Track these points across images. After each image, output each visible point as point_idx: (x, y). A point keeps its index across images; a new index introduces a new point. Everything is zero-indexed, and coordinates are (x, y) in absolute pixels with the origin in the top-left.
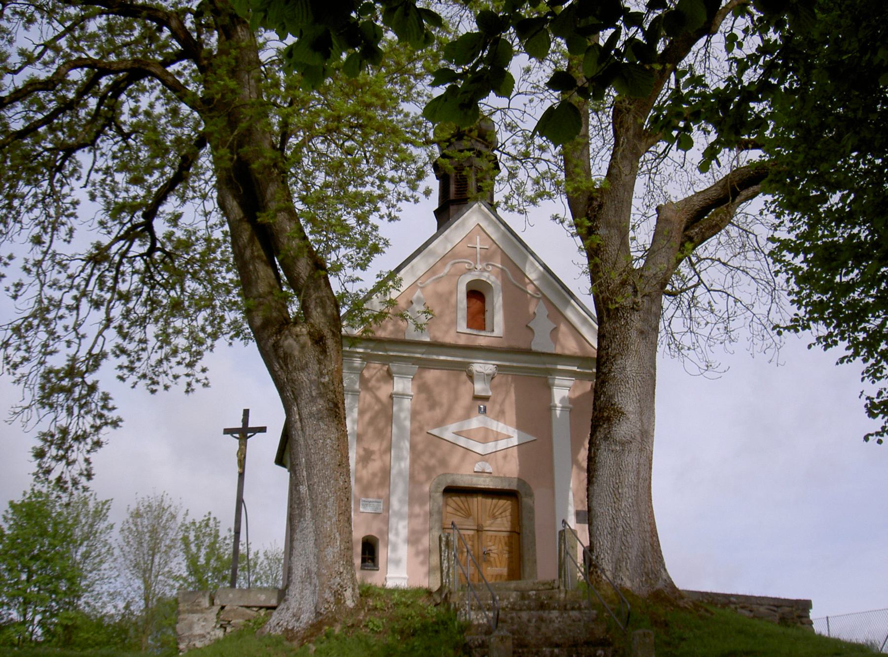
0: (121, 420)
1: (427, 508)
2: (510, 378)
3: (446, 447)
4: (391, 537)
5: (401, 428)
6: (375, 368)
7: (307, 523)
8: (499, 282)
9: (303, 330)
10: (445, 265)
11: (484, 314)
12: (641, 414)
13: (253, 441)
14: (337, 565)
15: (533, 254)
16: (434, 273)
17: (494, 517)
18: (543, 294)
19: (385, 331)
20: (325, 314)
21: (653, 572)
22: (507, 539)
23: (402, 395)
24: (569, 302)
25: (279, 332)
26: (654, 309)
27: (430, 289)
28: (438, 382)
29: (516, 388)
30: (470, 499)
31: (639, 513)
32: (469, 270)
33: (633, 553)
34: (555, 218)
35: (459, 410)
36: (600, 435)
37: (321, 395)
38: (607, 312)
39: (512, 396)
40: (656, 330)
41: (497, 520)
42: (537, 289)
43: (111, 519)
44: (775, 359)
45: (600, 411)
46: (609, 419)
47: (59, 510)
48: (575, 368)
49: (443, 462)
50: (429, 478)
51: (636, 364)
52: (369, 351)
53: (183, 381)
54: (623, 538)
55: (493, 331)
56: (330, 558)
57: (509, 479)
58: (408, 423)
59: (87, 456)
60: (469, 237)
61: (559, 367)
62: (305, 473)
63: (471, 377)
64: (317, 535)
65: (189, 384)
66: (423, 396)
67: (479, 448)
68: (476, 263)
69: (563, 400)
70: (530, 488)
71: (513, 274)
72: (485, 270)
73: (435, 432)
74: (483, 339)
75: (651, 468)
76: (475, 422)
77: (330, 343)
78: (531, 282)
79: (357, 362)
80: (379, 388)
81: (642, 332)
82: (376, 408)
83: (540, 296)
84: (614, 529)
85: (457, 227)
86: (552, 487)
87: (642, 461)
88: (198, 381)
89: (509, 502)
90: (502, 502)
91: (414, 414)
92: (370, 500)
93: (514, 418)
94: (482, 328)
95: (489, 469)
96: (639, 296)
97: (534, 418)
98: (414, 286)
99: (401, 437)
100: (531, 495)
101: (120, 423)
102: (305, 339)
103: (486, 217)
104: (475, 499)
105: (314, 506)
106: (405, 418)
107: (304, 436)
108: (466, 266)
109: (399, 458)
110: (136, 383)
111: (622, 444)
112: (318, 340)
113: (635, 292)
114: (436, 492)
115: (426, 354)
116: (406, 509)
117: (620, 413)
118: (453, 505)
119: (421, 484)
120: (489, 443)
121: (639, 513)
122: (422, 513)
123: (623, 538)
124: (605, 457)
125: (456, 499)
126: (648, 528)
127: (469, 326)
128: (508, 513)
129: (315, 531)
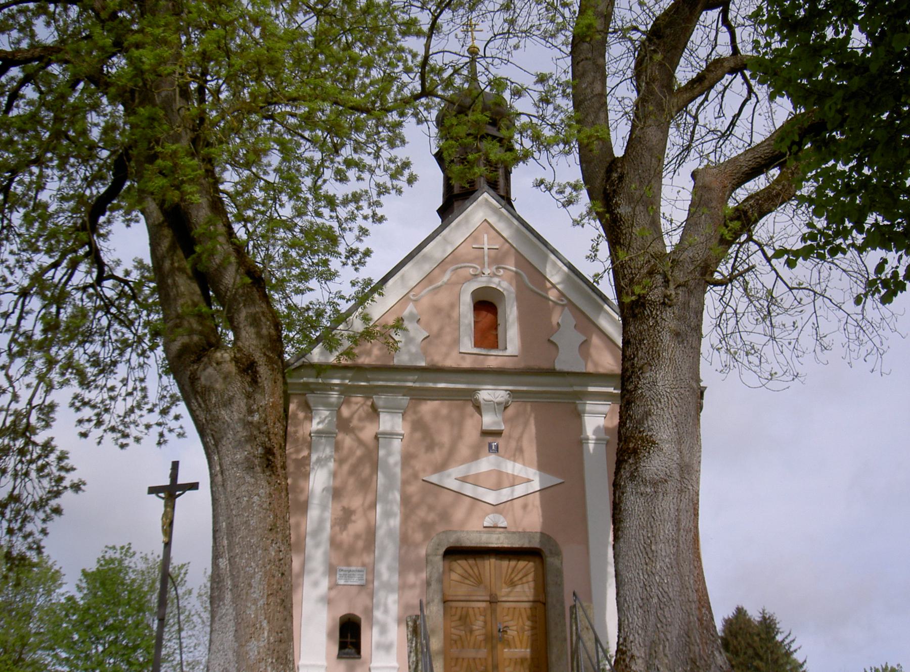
0: (84, 484)
1: (424, 575)
2: (529, 408)
3: (446, 498)
4: (378, 614)
5: (390, 476)
6: (357, 403)
7: (227, 609)
8: (513, 289)
9: (226, 355)
10: (444, 272)
11: (496, 329)
12: (680, 442)
13: (183, 501)
14: (263, 664)
15: (554, 252)
16: (431, 282)
17: (512, 584)
18: (569, 301)
19: (372, 354)
20: (259, 335)
21: (701, 657)
22: (529, 612)
23: (390, 435)
24: (602, 308)
25: (198, 360)
26: (693, 303)
27: (425, 302)
28: (436, 414)
29: (535, 418)
30: (480, 562)
31: (681, 576)
32: (475, 275)
33: (674, 633)
34: (540, 183)
35: (464, 450)
36: (625, 473)
37: (251, 439)
38: (632, 311)
39: (532, 428)
40: (698, 329)
41: (517, 589)
42: (562, 294)
43: (189, 585)
44: (878, 368)
45: (625, 441)
46: (635, 452)
47: (133, 577)
48: (611, 390)
49: (445, 516)
50: (427, 537)
51: (670, 377)
52: (347, 381)
53: (156, 430)
54: (660, 612)
55: (506, 348)
56: (253, 655)
57: (524, 533)
58: (398, 470)
59: (44, 526)
60: (474, 237)
61: (591, 389)
62: (225, 542)
63: (478, 408)
64: (237, 624)
65: (161, 435)
66: (418, 435)
67: (490, 497)
68: (483, 267)
69: (597, 431)
70: (557, 545)
71: (531, 277)
72: (495, 275)
73: (434, 478)
74: (493, 360)
75: (696, 515)
76: (486, 464)
77: (263, 370)
78: (554, 286)
79: (334, 396)
80: (361, 429)
81: (677, 334)
82: (359, 452)
83: (565, 302)
84: (646, 600)
85: (458, 225)
86: (585, 541)
87: (683, 506)
88: (171, 431)
89: (531, 564)
90: (522, 564)
91: (407, 458)
92: (353, 568)
93: (534, 456)
94: (495, 345)
95: (503, 523)
96: (672, 286)
97: (560, 455)
98: (405, 299)
99: (389, 488)
100: (558, 553)
101: (82, 486)
102: (231, 368)
103: (495, 211)
104: (487, 562)
105: (235, 586)
106: (396, 464)
107: (225, 493)
108: (471, 271)
109: (388, 515)
110: (101, 438)
111: (655, 484)
112: (248, 368)
113: (667, 282)
114: (436, 555)
115: (421, 382)
116: (395, 579)
117: (651, 443)
118: (459, 570)
119: (417, 546)
120: (502, 489)
121: (681, 576)
122: (418, 583)
123: (660, 612)
124: (633, 503)
125: (463, 563)
126: (694, 597)
127: (477, 345)
128: (530, 577)
129: (236, 618)
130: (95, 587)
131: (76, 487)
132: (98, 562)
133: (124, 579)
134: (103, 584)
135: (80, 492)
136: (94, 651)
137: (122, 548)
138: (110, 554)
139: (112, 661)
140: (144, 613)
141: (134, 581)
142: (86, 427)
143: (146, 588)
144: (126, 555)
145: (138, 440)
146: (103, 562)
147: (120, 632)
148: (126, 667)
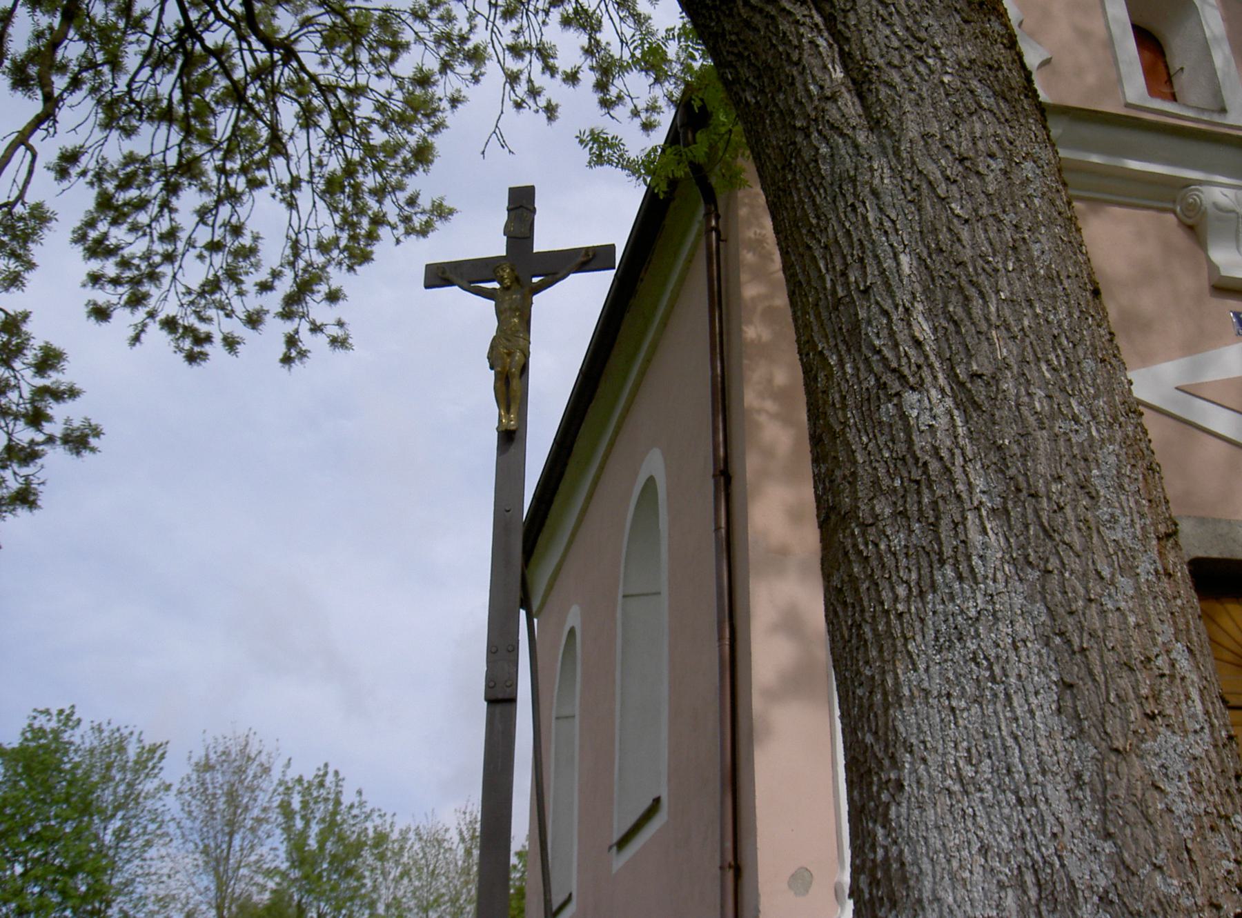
0: (97, 433)
47: (77, 759)
65: (292, 341)
88: (316, 329)
101: (93, 442)
130: (16, 774)
131: (78, 441)
132: (23, 734)
133: (62, 762)
134: (28, 769)
135: (86, 454)
136: (8, 873)
137: (61, 712)
138: (42, 721)
139: (37, 890)
140: (91, 816)
141: (76, 766)
142: (104, 296)
143: (95, 778)
144: (65, 724)
145: (231, 343)
146: (29, 735)
147: (52, 844)
148: (59, 899)
